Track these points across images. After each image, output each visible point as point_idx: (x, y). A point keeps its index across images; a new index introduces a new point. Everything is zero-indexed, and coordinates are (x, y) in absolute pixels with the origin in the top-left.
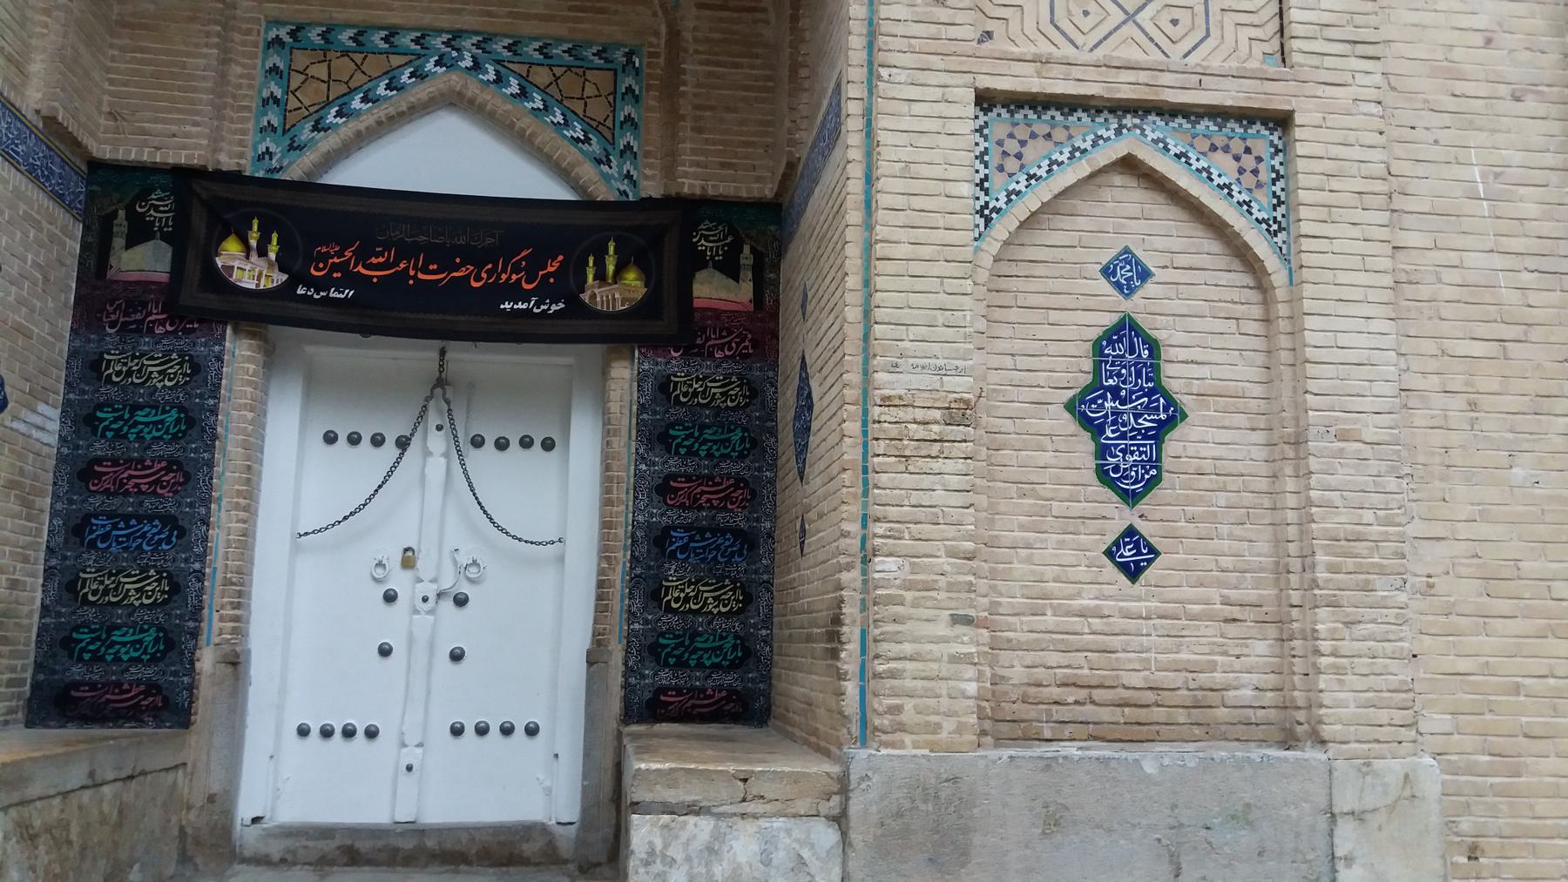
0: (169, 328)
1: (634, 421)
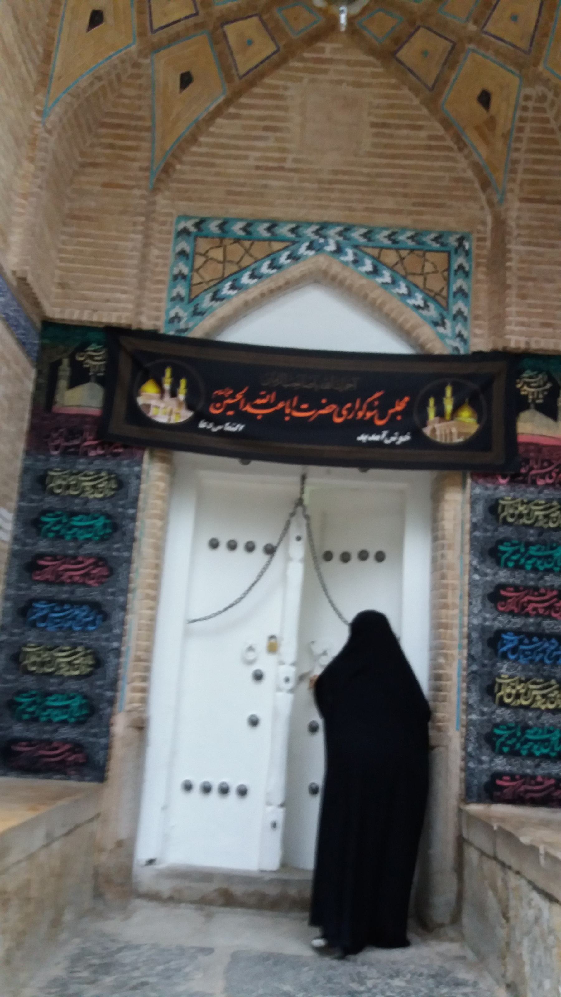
1: (467, 537)
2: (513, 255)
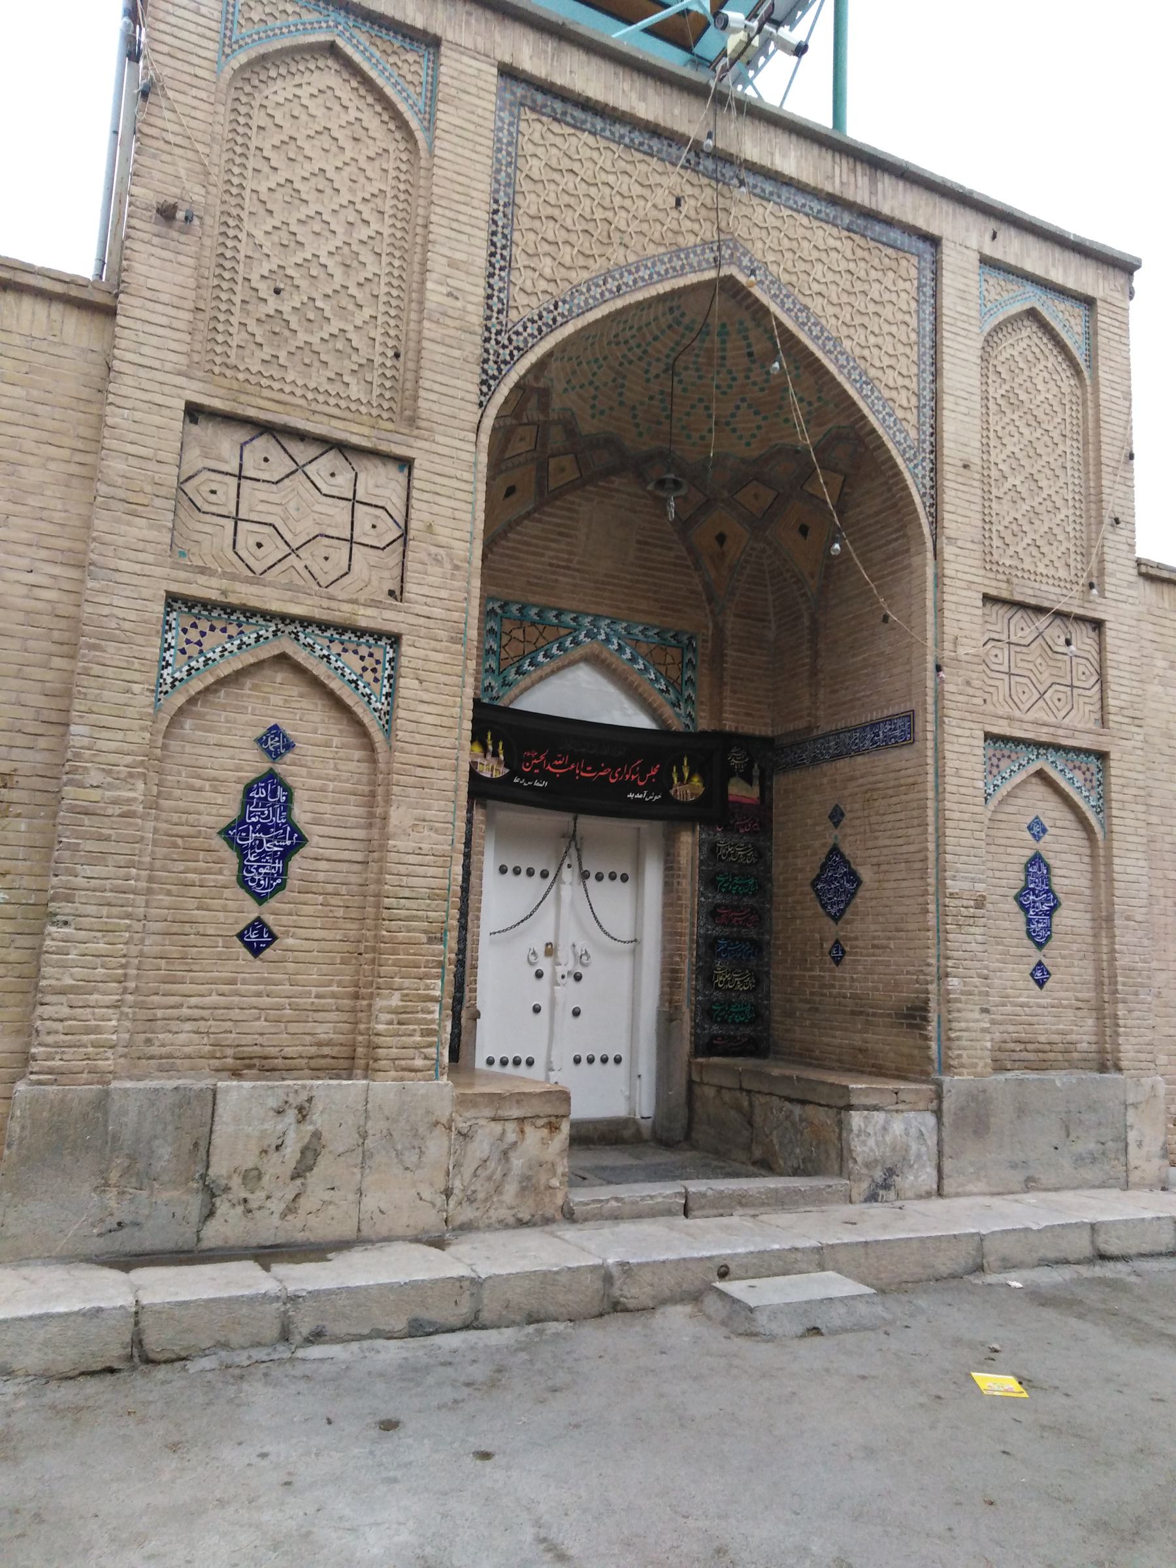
2: (728, 659)
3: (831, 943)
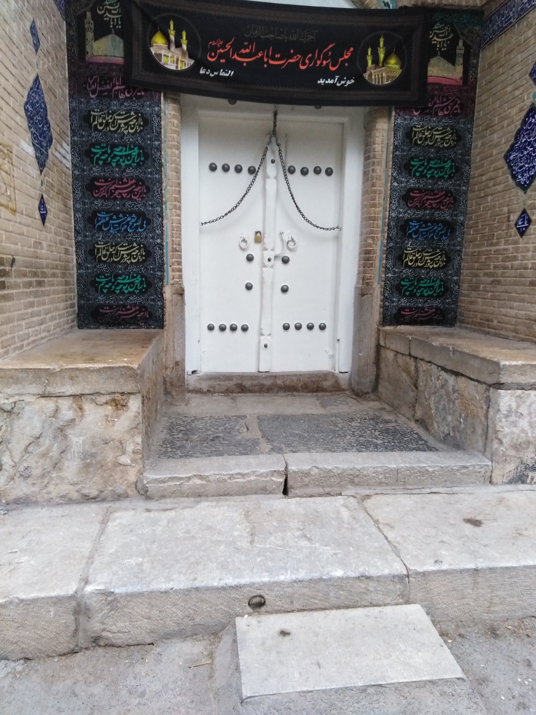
0: (128, 95)
1: (391, 156)
3: (518, 214)
